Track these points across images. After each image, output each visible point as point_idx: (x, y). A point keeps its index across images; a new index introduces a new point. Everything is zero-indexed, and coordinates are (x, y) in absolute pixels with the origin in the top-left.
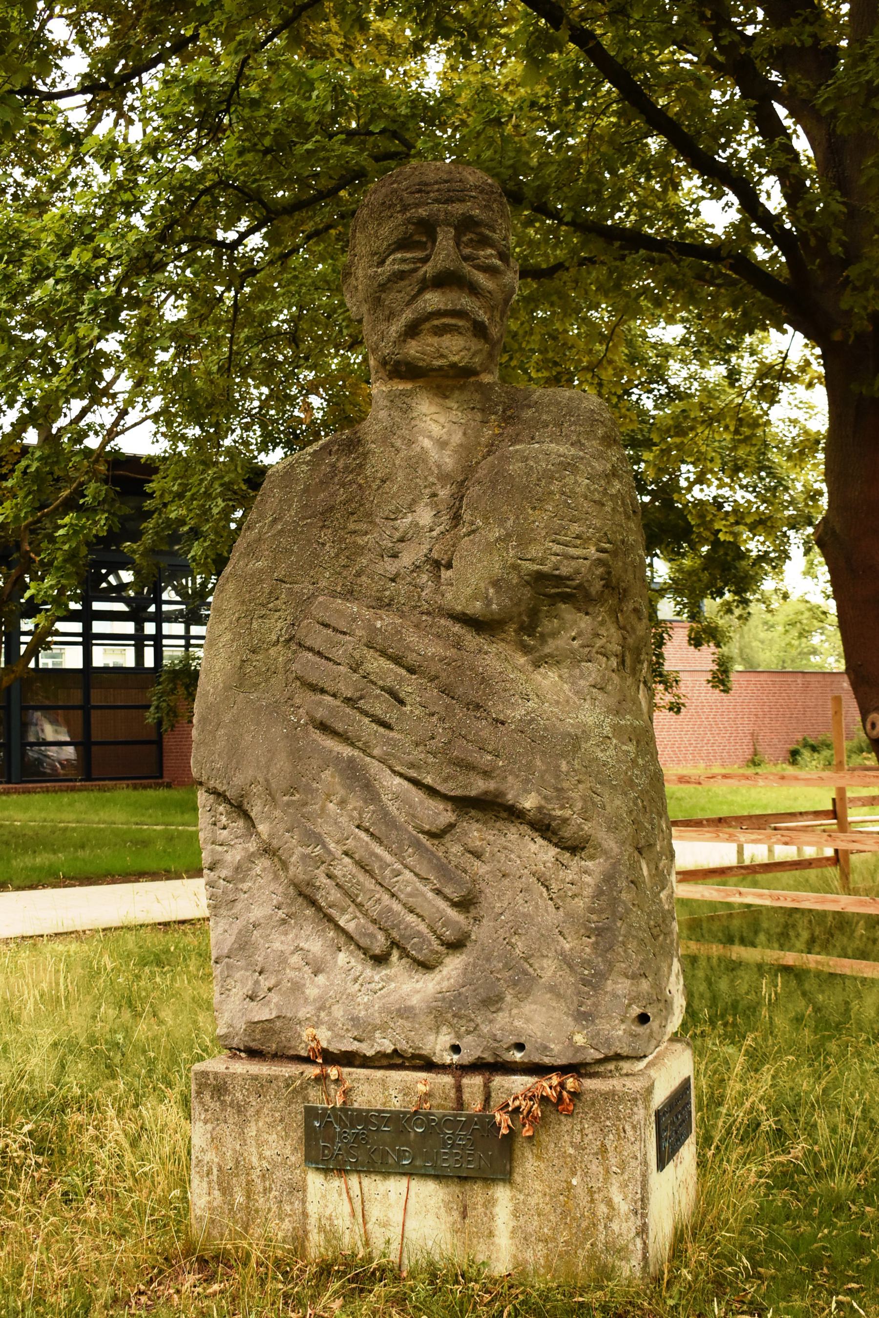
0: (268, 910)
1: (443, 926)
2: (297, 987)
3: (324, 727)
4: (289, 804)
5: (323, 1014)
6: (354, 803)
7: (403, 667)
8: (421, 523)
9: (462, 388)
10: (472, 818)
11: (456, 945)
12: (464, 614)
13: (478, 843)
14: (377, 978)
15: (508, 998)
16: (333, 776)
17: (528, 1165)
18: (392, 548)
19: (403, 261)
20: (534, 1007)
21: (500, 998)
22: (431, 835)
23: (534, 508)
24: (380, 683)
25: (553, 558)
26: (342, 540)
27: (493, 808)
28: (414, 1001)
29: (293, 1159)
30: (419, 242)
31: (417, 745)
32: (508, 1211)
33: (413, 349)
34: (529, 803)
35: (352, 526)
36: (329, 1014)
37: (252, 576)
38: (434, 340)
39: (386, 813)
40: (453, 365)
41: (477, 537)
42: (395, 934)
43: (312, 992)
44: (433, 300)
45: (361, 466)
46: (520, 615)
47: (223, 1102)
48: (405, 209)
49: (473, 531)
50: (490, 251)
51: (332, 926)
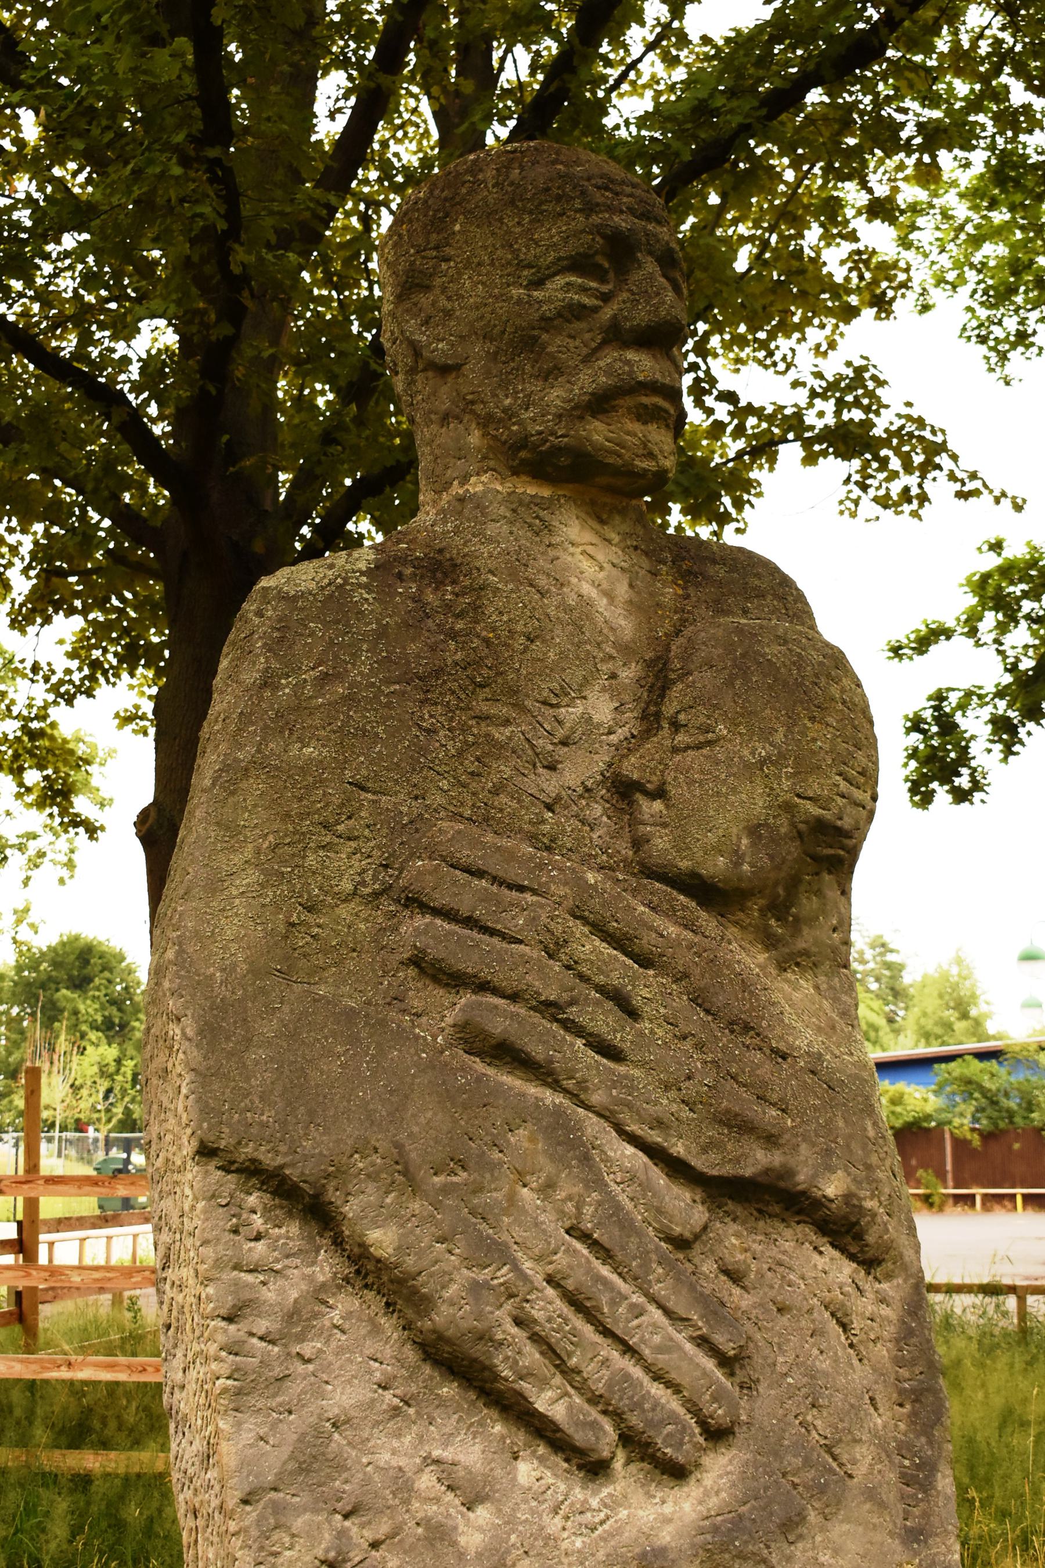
1: (715, 1399)
3: (506, 1053)
4: (446, 1190)
8: (596, 718)
9: (623, 512)
10: (727, 1213)
11: (717, 1434)
12: (694, 875)
13: (740, 1257)
14: (594, 1503)
15: (812, 1517)
16: (532, 1140)
18: (550, 753)
20: (846, 1527)
21: (802, 1518)
23: (813, 719)
24: (601, 979)
26: (465, 729)
27: (772, 1198)
28: (666, 1537)
30: (600, 266)
31: (667, 1088)
33: (597, 432)
35: (484, 707)
37: (303, 770)
39: (618, 1207)
42: (634, 1420)
46: (776, 884)
48: (590, 209)
49: (709, 743)
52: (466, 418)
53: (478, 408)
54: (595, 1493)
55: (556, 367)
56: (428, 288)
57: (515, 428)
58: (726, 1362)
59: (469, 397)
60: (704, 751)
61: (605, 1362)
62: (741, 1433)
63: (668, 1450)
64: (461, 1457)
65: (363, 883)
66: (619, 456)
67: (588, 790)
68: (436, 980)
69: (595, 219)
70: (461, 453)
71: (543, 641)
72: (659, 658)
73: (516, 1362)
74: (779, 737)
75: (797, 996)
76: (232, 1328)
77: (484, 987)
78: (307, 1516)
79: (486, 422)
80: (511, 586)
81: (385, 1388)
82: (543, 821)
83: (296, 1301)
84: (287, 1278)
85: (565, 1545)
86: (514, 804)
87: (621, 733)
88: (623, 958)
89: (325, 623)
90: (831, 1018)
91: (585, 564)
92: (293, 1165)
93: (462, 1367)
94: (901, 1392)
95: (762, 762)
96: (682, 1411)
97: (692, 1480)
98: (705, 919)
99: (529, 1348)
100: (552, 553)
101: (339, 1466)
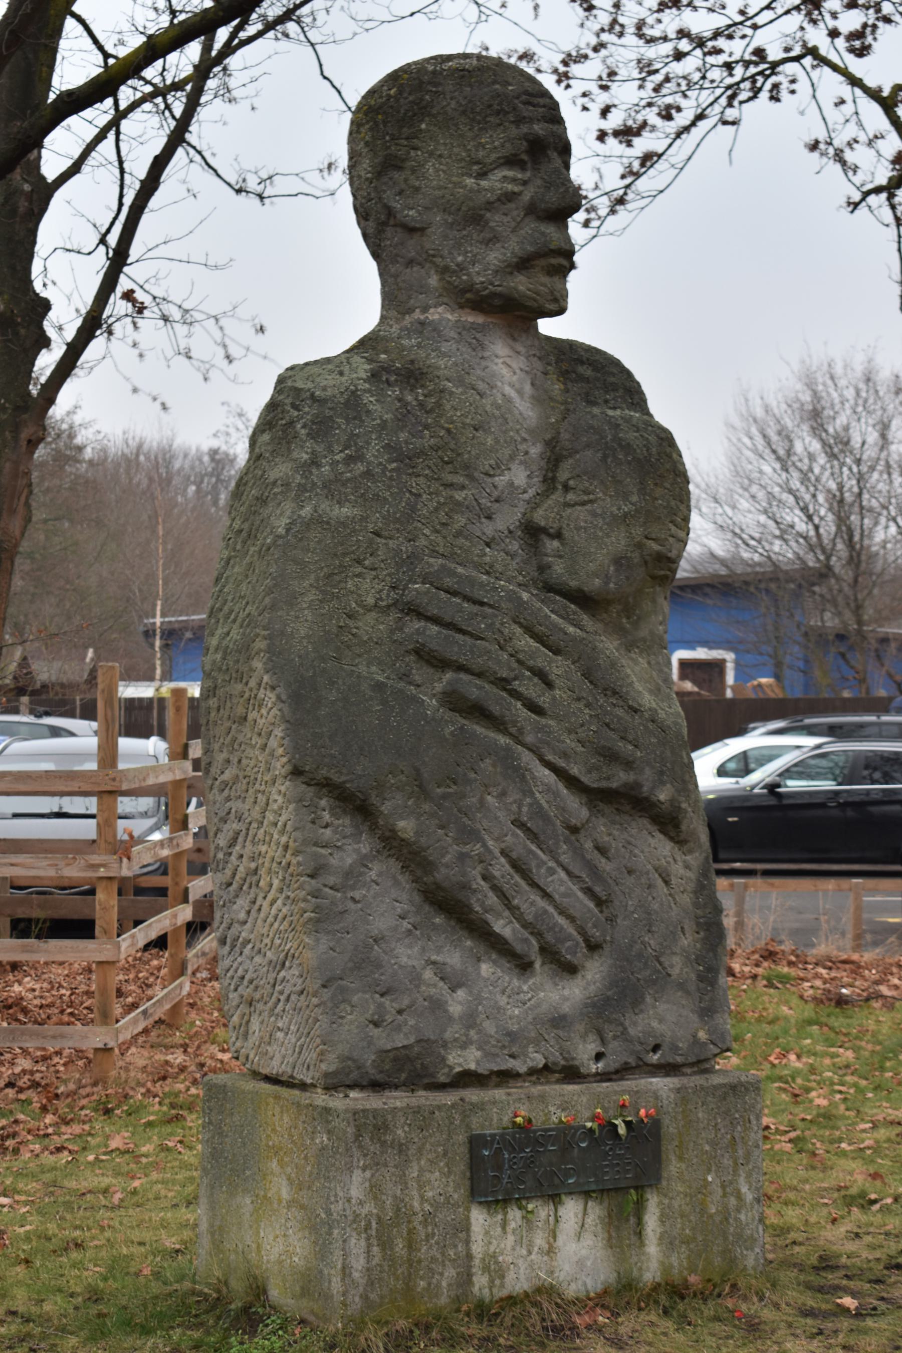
1: (595, 926)
2: (437, 1005)
3: (478, 711)
4: (445, 797)
5: (472, 1033)
11: (593, 947)
12: (580, 591)
13: (606, 839)
14: (525, 988)
16: (494, 766)
17: (672, 1168)
18: (489, 508)
19: (514, 180)
20: (666, 1006)
24: (531, 663)
28: (566, 1008)
29: (456, 1196)
31: (570, 733)
32: (655, 1218)
35: (450, 478)
39: (540, 807)
42: (549, 938)
43: (455, 1009)
47: (383, 1143)
52: (428, 265)
53: (438, 260)
54: (525, 982)
55: (495, 237)
56: (400, 168)
57: (465, 278)
58: (600, 903)
59: (431, 252)
60: (587, 507)
61: (532, 904)
62: (607, 948)
63: (568, 957)
64: (448, 960)
65: (381, 599)
66: (535, 300)
67: (510, 532)
68: (429, 663)
69: (524, 129)
70: (423, 289)
71: (484, 430)
72: (553, 438)
73: (484, 902)
74: (635, 498)
75: (637, 669)
76: (313, 882)
77: (461, 668)
78: (360, 995)
79: (444, 271)
80: (460, 390)
81: (403, 918)
82: (485, 554)
83: (351, 865)
84: (344, 851)
85: (509, 1013)
86: (468, 544)
87: (531, 492)
89: (347, 419)
90: (658, 684)
91: (505, 371)
92: (352, 781)
93: (449, 907)
94: (698, 924)
95: (626, 515)
96: (575, 933)
97: (579, 976)
98: (585, 619)
99: (491, 894)
100: (484, 363)
101: (378, 965)
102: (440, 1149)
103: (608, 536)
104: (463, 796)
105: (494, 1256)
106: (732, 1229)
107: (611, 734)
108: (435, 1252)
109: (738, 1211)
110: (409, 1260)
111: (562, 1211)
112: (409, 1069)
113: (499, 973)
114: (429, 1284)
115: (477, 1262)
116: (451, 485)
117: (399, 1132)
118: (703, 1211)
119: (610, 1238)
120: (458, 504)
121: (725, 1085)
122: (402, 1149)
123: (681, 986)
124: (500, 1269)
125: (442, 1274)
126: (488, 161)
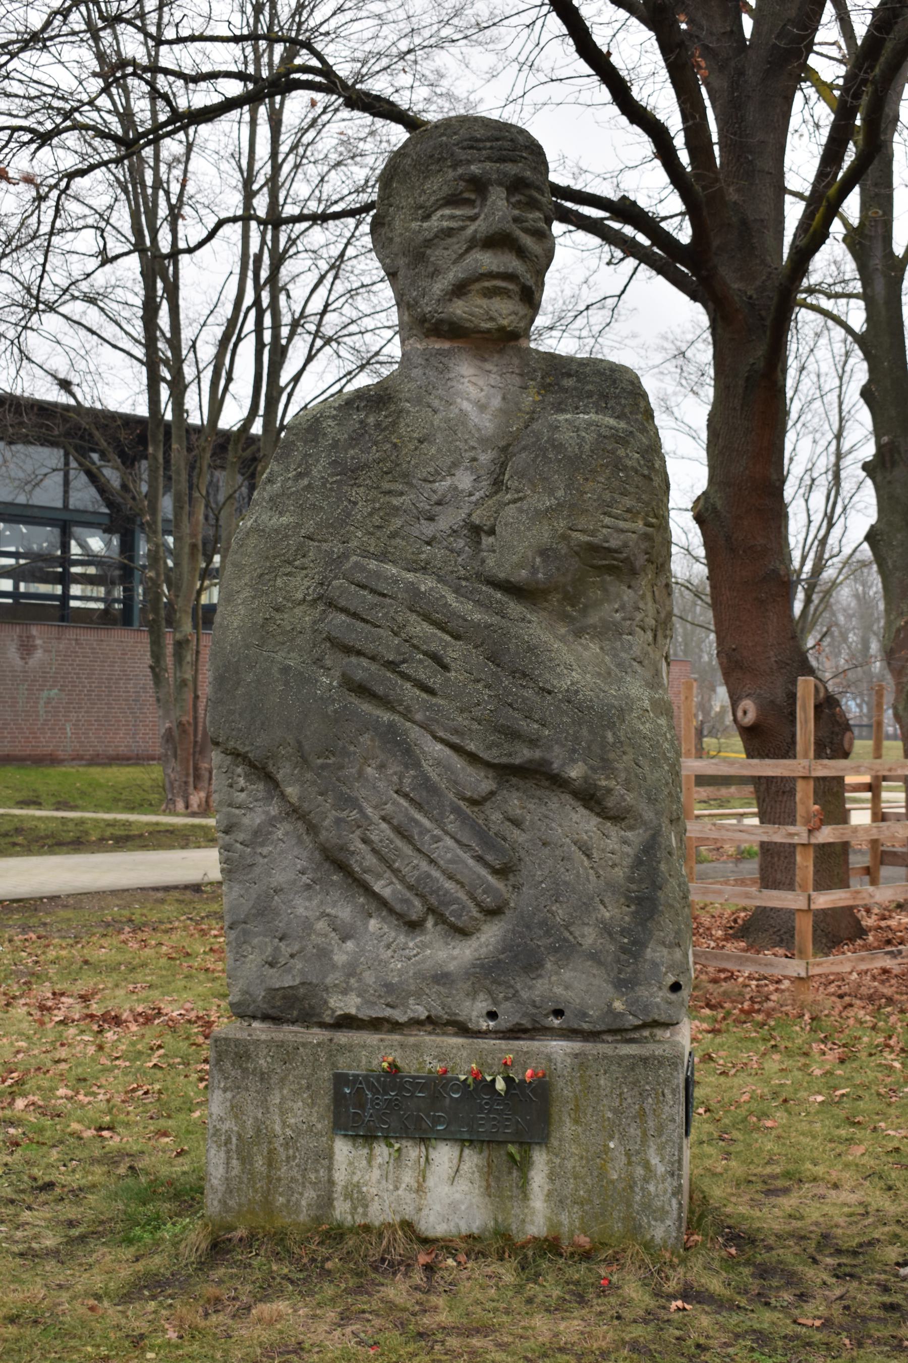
0: (291, 875)
1: (484, 892)
2: (324, 953)
3: (363, 690)
4: (323, 767)
5: (352, 981)
6: (394, 768)
7: (447, 632)
8: (461, 487)
11: (493, 913)
12: (508, 581)
13: (518, 811)
14: (411, 945)
15: (549, 965)
16: (372, 740)
19: (452, 217)
22: (473, 802)
24: (425, 647)
25: (604, 531)
27: (539, 776)
28: (452, 967)
29: (319, 1126)
31: (462, 711)
32: (543, 1175)
33: (459, 309)
34: (575, 772)
35: (386, 486)
36: (359, 980)
38: (484, 302)
39: (427, 779)
40: (502, 329)
41: (525, 505)
42: (433, 900)
43: (340, 958)
44: (487, 260)
45: (394, 424)
47: (245, 1070)
49: (520, 499)
50: (538, 215)
51: (361, 891)
69: (460, 171)
74: (560, 493)
75: (586, 654)
87: (478, 495)
88: (439, 633)
94: (628, 898)
95: (547, 510)
102: (304, 1082)
103: (529, 529)
104: (341, 767)
105: (358, 1185)
106: (638, 1198)
107: (516, 715)
108: (294, 1173)
109: (646, 1180)
110: (268, 1177)
111: (433, 1154)
112: (290, 1007)
113: (386, 928)
114: (289, 1201)
115: (339, 1188)
116: (389, 492)
117: (262, 1062)
118: (602, 1175)
119: (488, 1186)
120: (397, 509)
121: (634, 1057)
122: (263, 1077)
123: (594, 957)
124: (364, 1198)
125: (301, 1194)
126: (428, 204)
